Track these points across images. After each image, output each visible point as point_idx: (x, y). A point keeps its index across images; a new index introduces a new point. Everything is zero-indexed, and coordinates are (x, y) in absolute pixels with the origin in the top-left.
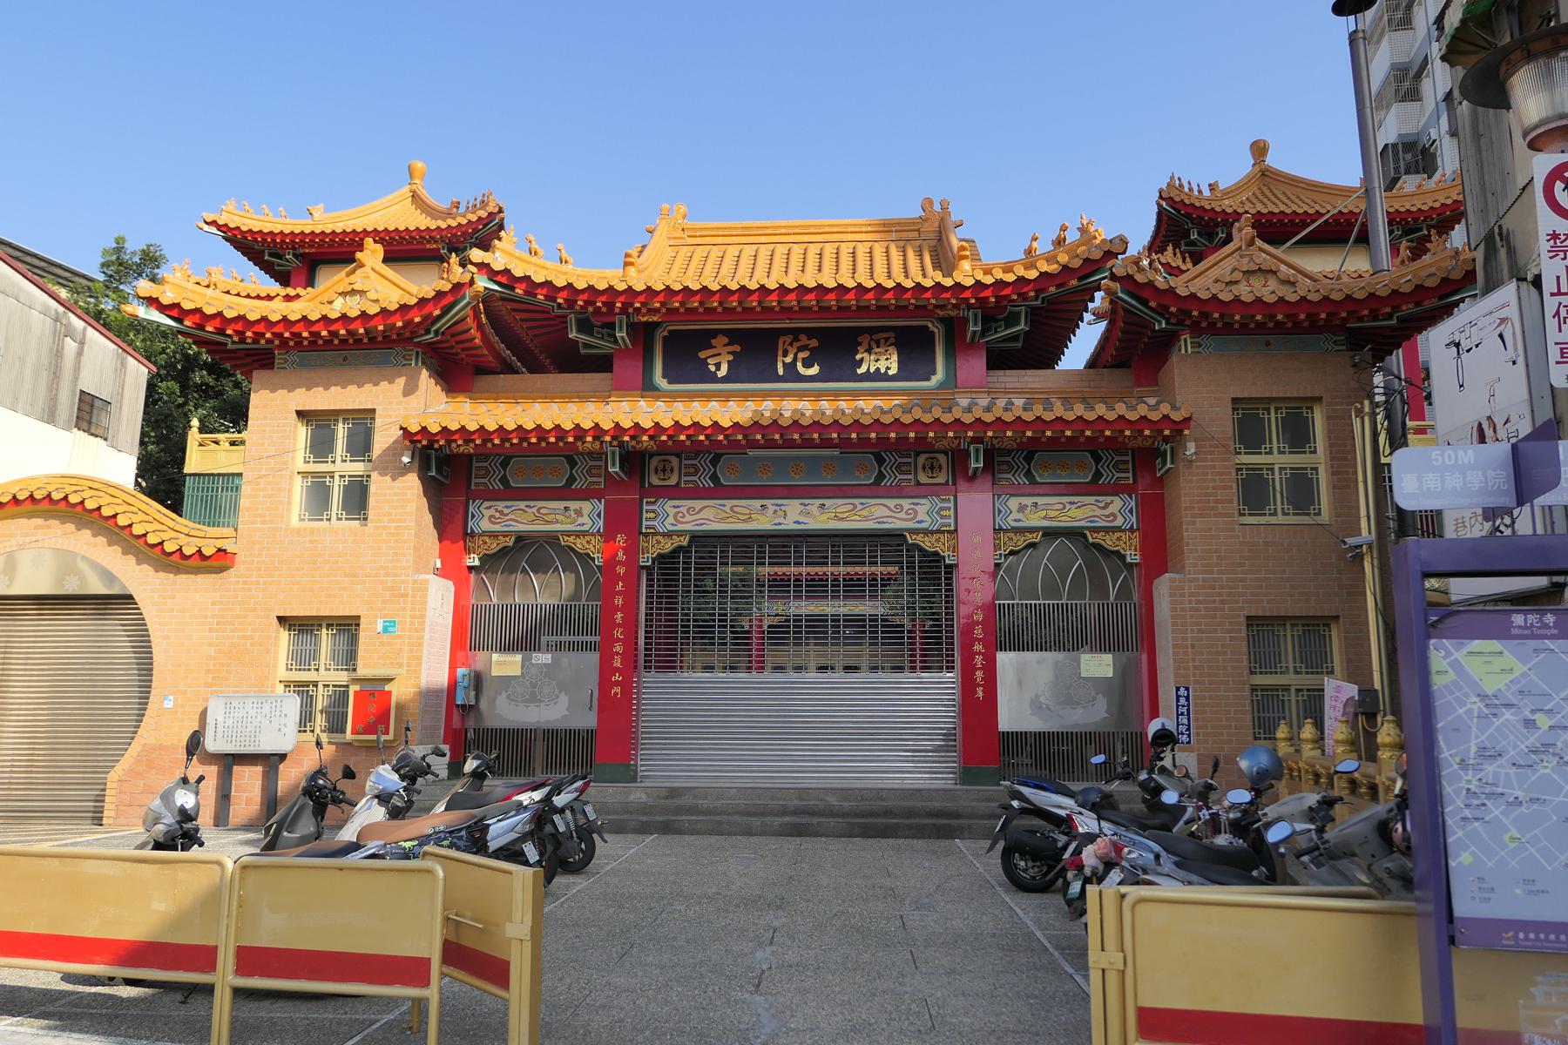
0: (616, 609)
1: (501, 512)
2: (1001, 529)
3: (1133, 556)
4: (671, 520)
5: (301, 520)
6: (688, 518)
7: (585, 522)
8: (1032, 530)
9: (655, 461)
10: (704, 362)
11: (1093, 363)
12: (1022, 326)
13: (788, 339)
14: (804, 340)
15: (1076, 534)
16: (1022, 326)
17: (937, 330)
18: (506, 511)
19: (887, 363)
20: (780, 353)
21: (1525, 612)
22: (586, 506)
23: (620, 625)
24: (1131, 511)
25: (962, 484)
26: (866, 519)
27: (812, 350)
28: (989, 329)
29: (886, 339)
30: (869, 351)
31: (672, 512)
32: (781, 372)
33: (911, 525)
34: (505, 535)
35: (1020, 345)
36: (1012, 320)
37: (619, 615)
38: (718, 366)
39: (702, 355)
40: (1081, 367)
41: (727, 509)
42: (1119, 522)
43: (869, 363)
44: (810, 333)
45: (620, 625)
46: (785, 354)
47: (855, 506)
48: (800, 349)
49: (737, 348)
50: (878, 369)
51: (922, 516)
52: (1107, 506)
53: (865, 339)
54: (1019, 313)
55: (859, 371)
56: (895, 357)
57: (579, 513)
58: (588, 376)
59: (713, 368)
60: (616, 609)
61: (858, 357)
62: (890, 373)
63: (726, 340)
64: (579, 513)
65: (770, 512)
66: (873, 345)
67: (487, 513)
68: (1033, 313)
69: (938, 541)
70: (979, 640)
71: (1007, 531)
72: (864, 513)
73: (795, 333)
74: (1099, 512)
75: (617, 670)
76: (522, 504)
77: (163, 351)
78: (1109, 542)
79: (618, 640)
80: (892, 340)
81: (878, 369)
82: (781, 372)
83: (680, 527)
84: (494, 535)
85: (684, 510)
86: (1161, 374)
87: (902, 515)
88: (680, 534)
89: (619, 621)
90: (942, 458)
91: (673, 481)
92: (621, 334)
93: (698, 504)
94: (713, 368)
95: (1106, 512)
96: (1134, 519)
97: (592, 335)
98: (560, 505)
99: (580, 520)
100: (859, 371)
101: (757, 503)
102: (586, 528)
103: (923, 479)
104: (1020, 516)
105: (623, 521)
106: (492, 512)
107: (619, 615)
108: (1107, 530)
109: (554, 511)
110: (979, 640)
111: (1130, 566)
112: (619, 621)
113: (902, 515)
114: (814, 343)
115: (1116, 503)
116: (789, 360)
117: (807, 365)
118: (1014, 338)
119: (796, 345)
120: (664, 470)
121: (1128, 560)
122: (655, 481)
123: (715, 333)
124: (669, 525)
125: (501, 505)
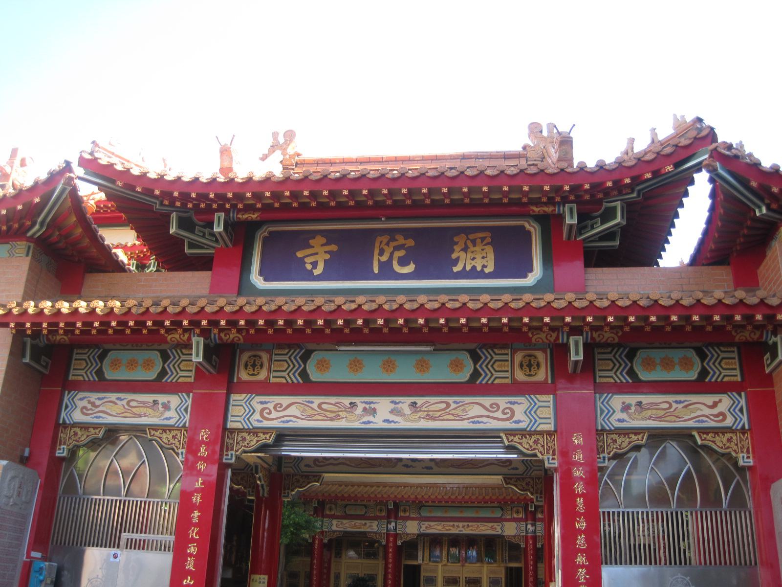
0: (193, 507)
1: (93, 404)
2: (603, 430)
3: (745, 460)
4: (257, 416)
5: (424, 576)
6: (275, 414)
7: (172, 417)
8: (637, 431)
9: (245, 357)
10: (302, 261)
11: (696, 260)
12: (618, 219)
13: (385, 239)
14: (401, 240)
15: (683, 436)
16: (618, 219)
17: (534, 230)
18: (98, 403)
19: (484, 262)
20: (376, 252)
21: (197, 557)
22: (174, 400)
23: (195, 525)
24: (741, 410)
25: (561, 383)
26: (458, 418)
27: (408, 250)
28: (585, 227)
29: (483, 239)
30: (465, 249)
31: (258, 407)
32: (376, 270)
33: (507, 425)
34: (96, 426)
35: (617, 243)
36: (609, 214)
37: (196, 514)
38: (315, 265)
39: (300, 254)
40: (687, 260)
41: (315, 406)
42: (729, 422)
43: (464, 261)
44: (407, 233)
45: (195, 525)
46: (381, 253)
47: (448, 405)
48: (397, 248)
49: (334, 248)
50: (474, 268)
51: (519, 415)
52: (715, 405)
53: (461, 239)
54: (615, 208)
55: (456, 269)
56: (491, 257)
57: (166, 407)
58: (189, 274)
59: (309, 267)
60: (193, 507)
61: (454, 256)
62: (487, 271)
63: (324, 240)
64: (166, 407)
65: (359, 410)
66: (469, 244)
67: (81, 404)
68: (630, 209)
69: (536, 442)
70: (582, 551)
71: (610, 432)
72: (457, 412)
73: (392, 233)
74: (707, 411)
75: (189, 572)
76: (113, 396)
77: (289, 516)
78: (719, 443)
79: (193, 540)
80: (489, 240)
81: (474, 268)
82: (376, 270)
83: (266, 424)
84: (85, 427)
85: (271, 406)
86: (762, 271)
87: (499, 415)
88: (266, 431)
89: (195, 520)
90: (540, 356)
91: (333, 513)
92: (218, 228)
93: (285, 400)
94: (309, 267)
95: (715, 411)
96: (745, 419)
97: (193, 232)
98: (149, 398)
99: (168, 414)
100: (456, 269)
101: (346, 400)
102: (172, 422)
103: (520, 376)
104: (624, 416)
105: (211, 411)
106: (84, 403)
107: (196, 514)
108: (717, 431)
109: (144, 404)
110: (582, 551)
111: (741, 470)
112: (195, 520)
113: (499, 415)
114: (410, 243)
115: (725, 402)
116: (384, 258)
117: (403, 262)
118: (608, 235)
119: (393, 244)
120: (254, 366)
121: (741, 463)
122: (328, 512)
123: (314, 234)
124: (256, 421)
125: (94, 396)
